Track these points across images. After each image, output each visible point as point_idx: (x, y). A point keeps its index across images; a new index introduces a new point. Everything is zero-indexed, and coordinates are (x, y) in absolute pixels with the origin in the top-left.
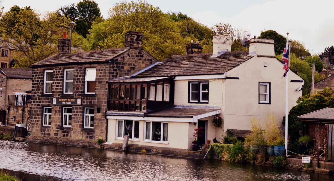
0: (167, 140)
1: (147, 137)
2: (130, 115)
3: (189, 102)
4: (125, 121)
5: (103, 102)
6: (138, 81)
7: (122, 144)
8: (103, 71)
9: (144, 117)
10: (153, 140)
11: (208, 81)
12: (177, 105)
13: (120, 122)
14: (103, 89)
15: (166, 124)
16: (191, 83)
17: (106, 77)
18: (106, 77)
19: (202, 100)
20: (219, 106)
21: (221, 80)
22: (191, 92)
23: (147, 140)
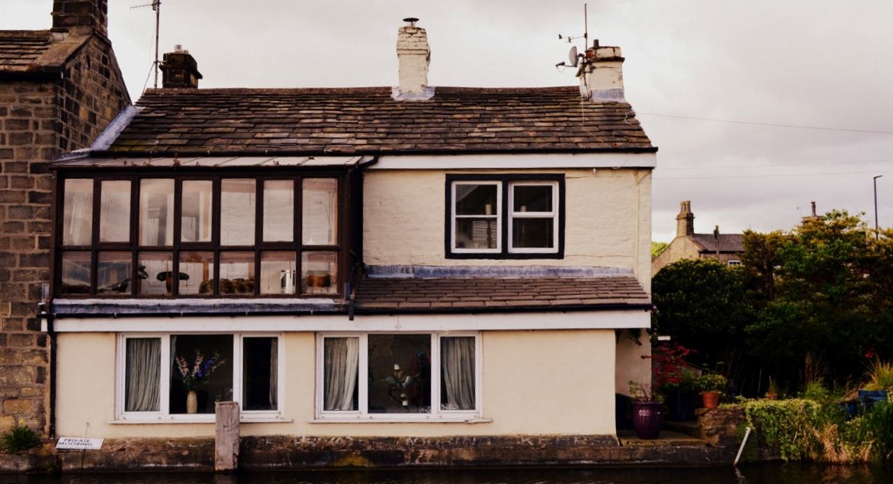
0: (473, 407)
2: (234, 311)
3: (449, 255)
4: (175, 339)
5: (13, 255)
6: (281, 164)
7: (209, 445)
8: (9, 117)
9: (351, 319)
10: (372, 409)
11: (564, 175)
12: (377, 267)
13: (131, 343)
14: (10, 197)
15: (460, 345)
16: (454, 185)
17: (33, 145)
18: (33, 145)
19: (514, 246)
20: (620, 266)
21: (631, 175)
22: (454, 216)
23: (345, 415)
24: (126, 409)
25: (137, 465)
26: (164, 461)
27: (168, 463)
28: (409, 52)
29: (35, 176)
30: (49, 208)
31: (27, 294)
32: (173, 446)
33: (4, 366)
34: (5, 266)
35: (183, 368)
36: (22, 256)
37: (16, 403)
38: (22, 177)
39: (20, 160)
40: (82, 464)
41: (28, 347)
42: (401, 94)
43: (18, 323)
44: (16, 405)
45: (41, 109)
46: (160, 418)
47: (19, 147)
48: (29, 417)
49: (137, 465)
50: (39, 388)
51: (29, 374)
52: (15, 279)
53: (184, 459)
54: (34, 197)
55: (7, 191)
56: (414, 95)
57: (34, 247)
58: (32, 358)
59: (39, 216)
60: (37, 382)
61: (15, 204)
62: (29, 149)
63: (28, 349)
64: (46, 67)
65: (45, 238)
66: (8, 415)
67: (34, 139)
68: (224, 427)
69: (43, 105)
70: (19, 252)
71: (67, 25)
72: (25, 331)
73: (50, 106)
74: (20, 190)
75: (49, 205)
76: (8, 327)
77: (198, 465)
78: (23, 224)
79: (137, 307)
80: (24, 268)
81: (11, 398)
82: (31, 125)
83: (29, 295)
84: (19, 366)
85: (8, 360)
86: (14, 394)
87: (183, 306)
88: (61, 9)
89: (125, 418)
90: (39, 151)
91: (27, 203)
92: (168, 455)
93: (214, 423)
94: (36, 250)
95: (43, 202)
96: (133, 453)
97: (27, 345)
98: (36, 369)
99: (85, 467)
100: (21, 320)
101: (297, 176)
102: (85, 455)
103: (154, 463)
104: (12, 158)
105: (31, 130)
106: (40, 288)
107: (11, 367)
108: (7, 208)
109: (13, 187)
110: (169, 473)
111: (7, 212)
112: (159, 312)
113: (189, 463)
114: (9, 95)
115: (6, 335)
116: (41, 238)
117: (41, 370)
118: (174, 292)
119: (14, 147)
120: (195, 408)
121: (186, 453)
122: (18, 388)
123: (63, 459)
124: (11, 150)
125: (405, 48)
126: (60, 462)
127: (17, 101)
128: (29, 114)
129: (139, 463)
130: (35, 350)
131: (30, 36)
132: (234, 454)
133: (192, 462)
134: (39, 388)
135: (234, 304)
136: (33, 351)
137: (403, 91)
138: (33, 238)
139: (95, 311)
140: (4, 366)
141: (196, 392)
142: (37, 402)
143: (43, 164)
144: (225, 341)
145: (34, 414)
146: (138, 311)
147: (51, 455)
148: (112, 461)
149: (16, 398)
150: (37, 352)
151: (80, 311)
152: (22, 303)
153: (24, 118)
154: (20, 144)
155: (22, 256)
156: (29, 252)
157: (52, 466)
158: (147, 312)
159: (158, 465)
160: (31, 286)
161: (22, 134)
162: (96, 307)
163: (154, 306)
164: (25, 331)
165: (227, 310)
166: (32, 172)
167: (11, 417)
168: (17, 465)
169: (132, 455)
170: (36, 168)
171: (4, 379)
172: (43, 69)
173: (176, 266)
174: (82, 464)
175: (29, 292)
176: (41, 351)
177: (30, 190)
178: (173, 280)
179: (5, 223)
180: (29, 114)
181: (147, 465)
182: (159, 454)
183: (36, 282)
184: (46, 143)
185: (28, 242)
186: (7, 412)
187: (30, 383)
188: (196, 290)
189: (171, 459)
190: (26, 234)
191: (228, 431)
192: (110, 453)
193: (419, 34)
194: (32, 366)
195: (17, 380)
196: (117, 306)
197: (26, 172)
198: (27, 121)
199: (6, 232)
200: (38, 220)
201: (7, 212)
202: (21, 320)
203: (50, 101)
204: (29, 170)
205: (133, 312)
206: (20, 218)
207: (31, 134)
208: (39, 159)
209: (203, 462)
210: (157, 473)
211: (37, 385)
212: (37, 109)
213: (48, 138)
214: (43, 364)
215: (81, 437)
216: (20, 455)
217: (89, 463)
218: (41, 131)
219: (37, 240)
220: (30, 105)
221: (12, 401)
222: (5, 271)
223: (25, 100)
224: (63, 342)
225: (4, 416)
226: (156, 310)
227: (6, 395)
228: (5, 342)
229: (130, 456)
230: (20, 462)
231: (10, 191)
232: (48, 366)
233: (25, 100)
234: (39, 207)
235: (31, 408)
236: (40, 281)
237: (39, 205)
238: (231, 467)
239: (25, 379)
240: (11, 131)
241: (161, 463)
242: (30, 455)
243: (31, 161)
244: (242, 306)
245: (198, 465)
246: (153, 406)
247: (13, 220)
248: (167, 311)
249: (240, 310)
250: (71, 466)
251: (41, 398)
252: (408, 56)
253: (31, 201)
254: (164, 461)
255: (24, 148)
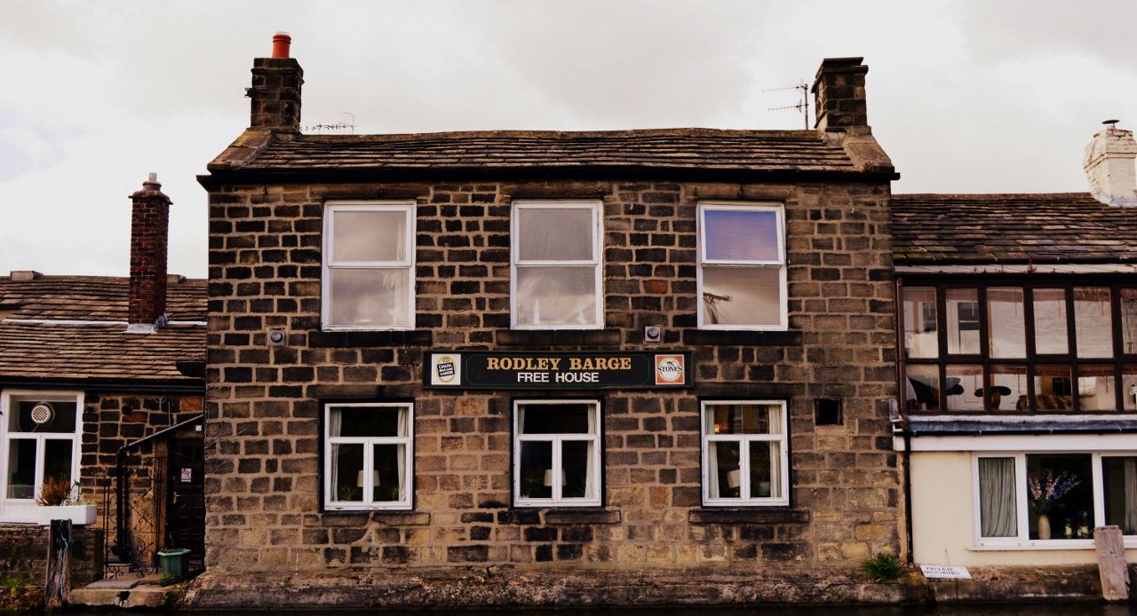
1: (993, 522)
2: (1105, 427)
5: (857, 368)
7: (1093, 572)
8: (844, 220)
14: (851, 306)
18: (870, 250)
24: (983, 536)
25: (1014, 595)
26: (1043, 591)
27: (1048, 593)
28: (1118, 155)
29: (874, 283)
30: (891, 318)
31: (873, 410)
32: (1046, 574)
33: (854, 489)
34: (849, 380)
35: (1036, 490)
36: (867, 369)
37: (868, 529)
38: (861, 284)
39: (859, 267)
40: (957, 594)
41: (877, 468)
42: (1113, 200)
43: (867, 441)
44: (869, 531)
45: (876, 212)
46: (1020, 544)
47: (856, 252)
48: (883, 544)
49: (1014, 595)
50: (891, 512)
51: (880, 497)
52: (861, 395)
53: (1065, 589)
54: (875, 306)
55: (847, 299)
56: (1127, 201)
57: (878, 360)
58: (883, 480)
59: (881, 326)
60: (889, 506)
61: (856, 314)
62: (867, 254)
63: (878, 470)
64: (400, 183)
65: (889, 349)
66: (861, 541)
67: (871, 243)
68: (1111, 553)
69: (878, 207)
70: (862, 365)
71: (842, 124)
72: (874, 450)
73: (885, 209)
74: (860, 298)
75: (892, 315)
76: (856, 446)
77: (1079, 595)
78: (866, 335)
79: (1001, 424)
80: (869, 383)
81: (863, 523)
82: (867, 229)
83: (877, 412)
84: (870, 489)
85: (857, 482)
86: (866, 518)
87: (1049, 423)
88: (835, 108)
89: (982, 544)
90: (877, 257)
91: (868, 313)
92: (1046, 584)
93: (1094, 550)
94: (881, 363)
95: (885, 312)
96: (1009, 582)
97: (875, 466)
98: (887, 491)
99: (960, 597)
100: (869, 438)
101: (1069, 286)
102: (958, 584)
103: (1032, 593)
104: (850, 265)
105: (867, 234)
106: (888, 404)
107: (862, 489)
108: (848, 317)
109: (853, 294)
110: (1050, 604)
111: (848, 322)
112: (1023, 429)
113: (1070, 592)
114: (842, 197)
115: (854, 454)
116: (885, 351)
117: (892, 492)
118: (992, 407)
119: (852, 253)
120: (1049, 535)
121: (1065, 582)
122: (870, 512)
123: (936, 588)
124: (849, 256)
125: (1116, 151)
126: (931, 592)
127: (851, 203)
128: (864, 217)
129: (1017, 593)
130: (885, 471)
131: (788, 136)
132: (1127, 583)
133: (1073, 592)
134: (891, 512)
135: (1105, 421)
136: (884, 472)
137: (1115, 196)
138: (876, 350)
139: (955, 429)
140: (854, 489)
141: (1048, 516)
142: (891, 527)
143: (882, 270)
144: (1084, 459)
145: (887, 541)
146: (1001, 429)
147: (923, 585)
148: (988, 590)
149: (868, 523)
150: (887, 473)
151: (937, 428)
152: (869, 421)
153: (860, 221)
154: (857, 249)
155: (867, 369)
156: (874, 364)
157: (924, 597)
158: (1010, 429)
159: (1038, 595)
160: (878, 401)
161: (858, 239)
162: (955, 424)
163: (1020, 423)
164: (874, 450)
165: (1096, 427)
166: (871, 279)
167: (864, 544)
168: (888, 595)
169: (1009, 585)
170: (875, 275)
171: (855, 502)
172: (878, 169)
173: (987, 380)
174: (957, 594)
175: (876, 408)
176: (891, 472)
177: (870, 298)
178: (992, 396)
179: (846, 334)
180: (864, 217)
181: (1026, 595)
182: (1036, 583)
183: (883, 397)
184: (884, 248)
185: (871, 354)
186: (859, 538)
187: (882, 506)
188: (1014, 407)
189: (1049, 588)
190: (869, 346)
191: (1116, 557)
192: (985, 582)
193: (1127, 137)
194: (884, 489)
195: (869, 503)
196: (979, 423)
197: (864, 279)
198: (863, 225)
199: (848, 343)
200: (880, 330)
201: (848, 322)
202: (869, 438)
203: (885, 204)
204: (868, 277)
205: (996, 429)
206: (862, 328)
207: (868, 239)
208: (878, 266)
209: (1083, 592)
210: (1036, 604)
211: (890, 509)
212: (872, 211)
213: (886, 243)
214: (894, 486)
215: (939, 565)
216: (888, 584)
217: (963, 593)
218: (877, 236)
219: (881, 352)
220: (864, 207)
221: (864, 527)
222: (849, 385)
223: (860, 202)
224: (914, 460)
225: (856, 543)
226: (1020, 427)
227: (858, 520)
228: (853, 463)
229: (1006, 585)
230: (890, 592)
231: (851, 300)
232: (900, 489)
233: (860, 202)
234: (881, 317)
235: (884, 533)
236: (886, 397)
237: (881, 315)
238: (1126, 597)
239: (876, 502)
240: (847, 236)
241: (1040, 593)
242: (901, 585)
243: (869, 268)
244: (1112, 422)
245: (1079, 595)
246: (1009, 531)
247: (856, 331)
248: (1032, 429)
249: (1109, 427)
250: (946, 597)
251: (893, 522)
252: (1117, 160)
253: (872, 311)
254: (1043, 591)
255: (862, 254)
